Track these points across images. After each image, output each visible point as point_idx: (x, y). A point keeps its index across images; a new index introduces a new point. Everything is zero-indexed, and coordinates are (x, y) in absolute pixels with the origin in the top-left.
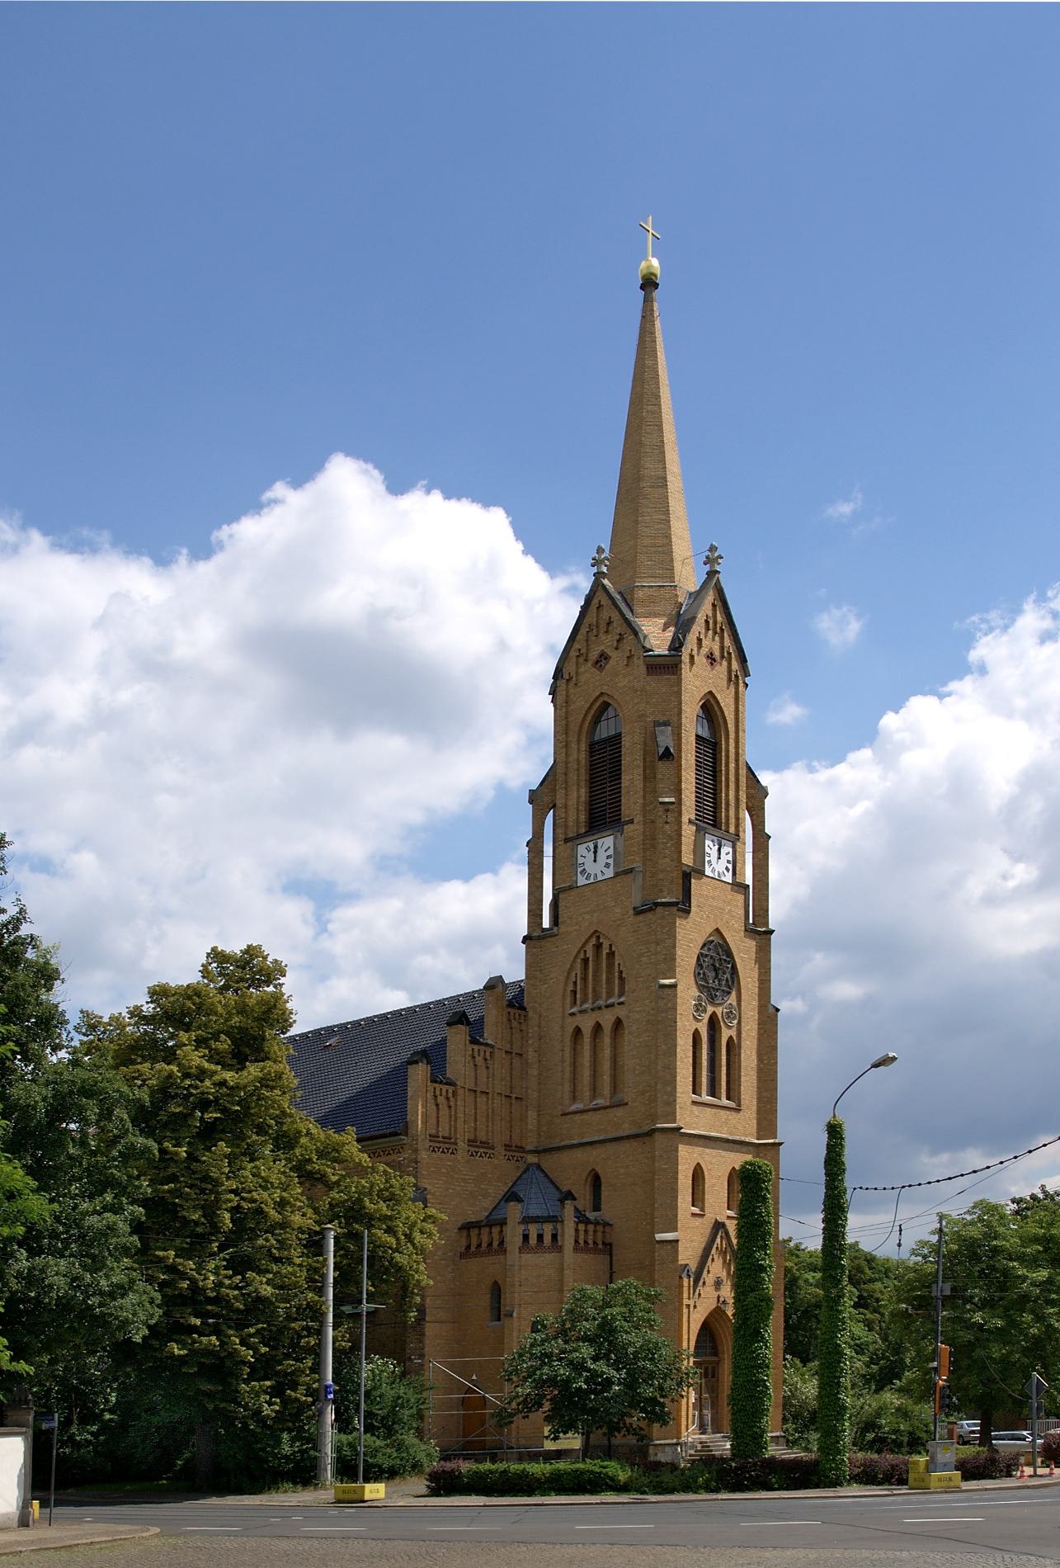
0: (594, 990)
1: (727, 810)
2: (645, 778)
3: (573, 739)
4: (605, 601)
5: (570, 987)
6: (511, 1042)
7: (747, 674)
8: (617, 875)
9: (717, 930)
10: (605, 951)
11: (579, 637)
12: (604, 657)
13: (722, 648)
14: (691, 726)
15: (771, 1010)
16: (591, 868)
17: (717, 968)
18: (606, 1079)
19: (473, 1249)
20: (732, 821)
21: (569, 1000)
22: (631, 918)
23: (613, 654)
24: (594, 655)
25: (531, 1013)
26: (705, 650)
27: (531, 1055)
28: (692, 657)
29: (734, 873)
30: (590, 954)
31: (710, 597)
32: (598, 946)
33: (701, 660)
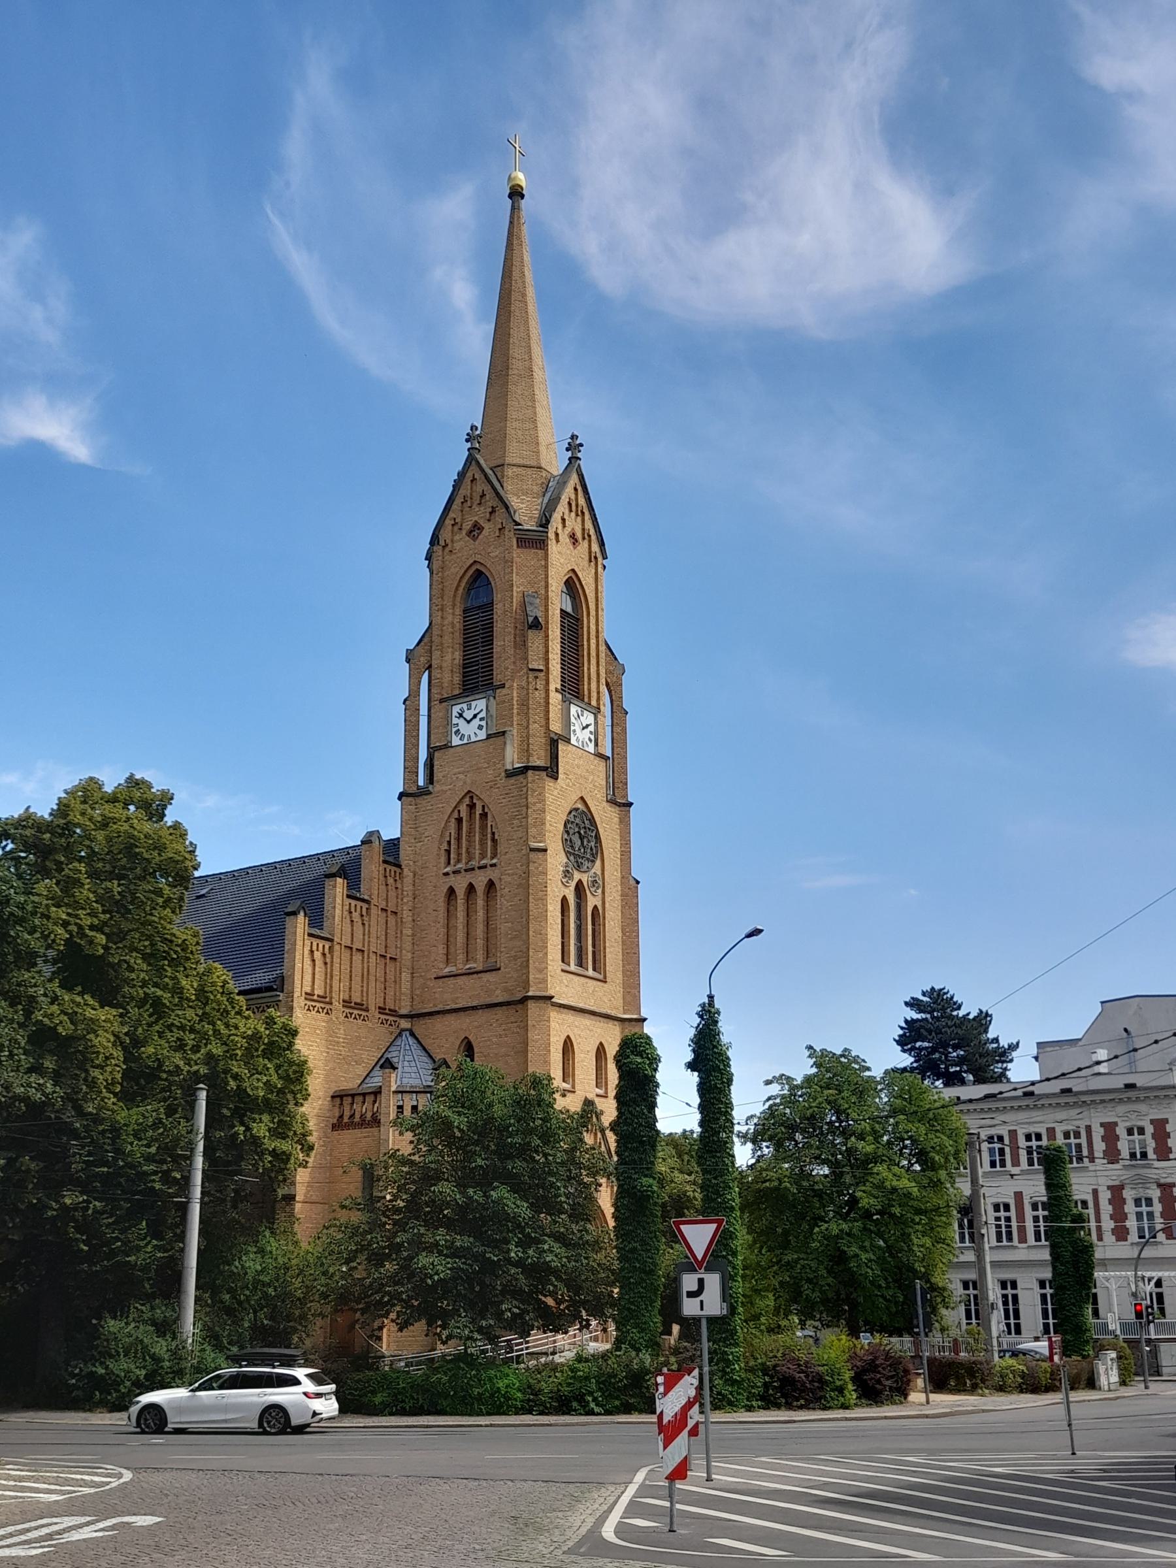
1: (589, 684)
3: (448, 602)
7: (605, 557)
8: (489, 737)
9: (582, 798)
10: (479, 811)
11: (454, 507)
12: (476, 528)
13: (583, 529)
14: (558, 601)
15: (633, 882)
17: (582, 835)
19: (346, 1120)
20: (594, 694)
21: (443, 859)
22: (503, 781)
24: (467, 526)
26: (568, 530)
27: (407, 915)
28: (557, 535)
29: (596, 745)
30: (464, 814)
31: (574, 479)
32: (472, 806)
33: (564, 538)
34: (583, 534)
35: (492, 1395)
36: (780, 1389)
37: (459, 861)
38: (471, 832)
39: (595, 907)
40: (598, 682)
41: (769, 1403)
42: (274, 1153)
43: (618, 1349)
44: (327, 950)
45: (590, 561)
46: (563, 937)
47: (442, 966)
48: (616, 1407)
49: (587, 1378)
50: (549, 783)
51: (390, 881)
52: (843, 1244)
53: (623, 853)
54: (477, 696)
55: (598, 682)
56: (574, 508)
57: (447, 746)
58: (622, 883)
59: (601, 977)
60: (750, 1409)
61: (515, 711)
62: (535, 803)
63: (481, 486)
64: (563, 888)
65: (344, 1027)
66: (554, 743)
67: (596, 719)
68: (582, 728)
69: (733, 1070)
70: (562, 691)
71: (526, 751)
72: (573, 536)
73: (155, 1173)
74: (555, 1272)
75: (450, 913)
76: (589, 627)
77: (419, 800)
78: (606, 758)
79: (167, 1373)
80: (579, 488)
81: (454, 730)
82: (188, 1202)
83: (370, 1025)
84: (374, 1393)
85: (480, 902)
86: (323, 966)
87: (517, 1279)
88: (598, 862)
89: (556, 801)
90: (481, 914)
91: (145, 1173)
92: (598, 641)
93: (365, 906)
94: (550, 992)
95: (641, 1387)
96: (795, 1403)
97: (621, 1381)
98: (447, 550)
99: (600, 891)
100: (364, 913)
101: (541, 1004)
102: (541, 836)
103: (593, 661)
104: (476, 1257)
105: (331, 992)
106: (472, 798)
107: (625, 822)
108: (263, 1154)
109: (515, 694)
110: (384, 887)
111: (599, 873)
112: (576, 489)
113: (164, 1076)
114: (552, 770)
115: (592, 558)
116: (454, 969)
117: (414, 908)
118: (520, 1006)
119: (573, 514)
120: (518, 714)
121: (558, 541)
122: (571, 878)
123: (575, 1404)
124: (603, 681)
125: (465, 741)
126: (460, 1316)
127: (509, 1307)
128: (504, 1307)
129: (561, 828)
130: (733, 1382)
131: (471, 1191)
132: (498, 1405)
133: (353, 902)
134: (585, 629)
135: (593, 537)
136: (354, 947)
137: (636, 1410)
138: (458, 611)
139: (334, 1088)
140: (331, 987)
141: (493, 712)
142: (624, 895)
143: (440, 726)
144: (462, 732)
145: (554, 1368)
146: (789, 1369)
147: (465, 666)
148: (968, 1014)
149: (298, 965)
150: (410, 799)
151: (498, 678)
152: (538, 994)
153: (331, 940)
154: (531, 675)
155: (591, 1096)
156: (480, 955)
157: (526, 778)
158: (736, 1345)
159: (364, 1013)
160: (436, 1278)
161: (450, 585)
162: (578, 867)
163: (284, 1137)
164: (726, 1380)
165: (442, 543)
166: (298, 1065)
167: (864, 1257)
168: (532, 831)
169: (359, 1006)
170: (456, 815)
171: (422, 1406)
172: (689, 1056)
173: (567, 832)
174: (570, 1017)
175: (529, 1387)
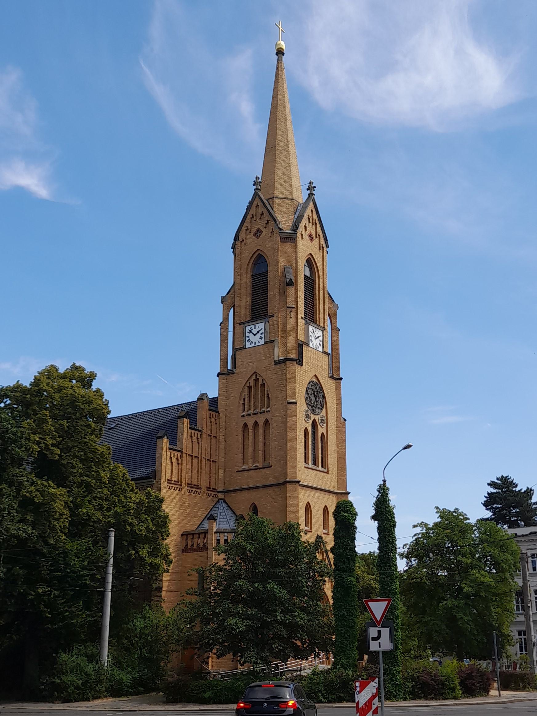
1: (319, 314)
5: (242, 401)
7: (328, 247)
8: (266, 343)
9: (315, 376)
10: (260, 382)
11: (247, 220)
12: (259, 232)
13: (316, 232)
14: (303, 271)
15: (343, 420)
17: (316, 396)
18: (261, 453)
19: (189, 547)
20: (322, 320)
21: (241, 408)
22: (273, 366)
23: (264, 230)
24: (254, 230)
25: (221, 415)
26: (308, 232)
27: (222, 438)
28: (302, 235)
29: (323, 347)
31: (311, 205)
32: (256, 380)
33: (306, 236)
37: (249, 409)
41: (415, 696)
42: (151, 565)
45: (320, 249)
46: (305, 450)
47: (240, 465)
48: (334, 699)
49: (318, 684)
50: (298, 367)
51: (213, 420)
57: (243, 348)
58: (337, 421)
59: (326, 471)
60: (405, 699)
63: (261, 209)
64: (305, 424)
66: (300, 346)
68: (316, 338)
70: (305, 318)
71: (285, 350)
72: (310, 236)
73: (87, 575)
76: (319, 285)
77: (228, 377)
78: (328, 354)
80: (314, 210)
81: (247, 339)
82: (105, 591)
84: (205, 692)
88: (324, 410)
89: (302, 377)
92: (324, 292)
93: (199, 433)
94: (299, 479)
98: (243, 243)
99: (325, 425)
101: (294, 485)
103: (322, 302)
105: (181, 479)
106: (256, 375)
107: (338, 388)
109: (280, 320)
111: (325, 415)
113: (92, 524)
114: (299, 361)
115: (321, 248)
116: (247, 467)
117: (225, 434)
118: (282, 486)
119: (311, 224)
120: (281, 331)
121: (302, 238)
122: (310, 418)
125: (253, 345)
128: (274, 646)
134: (317, 285)
135: (322, 236)
136: (194, 455)
138: (249, 276)
139: (183, 530)
140: (181, 476)
141: (268, 329)
143: (240, 337)
148: (521, 490)
151: (270, 312)
152: (292, 480)
153: (182, 452)
154: (288, 310)
155: (320, 534)
156: (261, 459)
157: (285, 365)
158: (398, 666)
159: (199, 491)
161: (245, 261)
162: (314, 412)
163: (157, 556)
168: (289, 393)
169: (196, 486)
172: (373, 513)
173: (308, 393)
174: (309, 492)
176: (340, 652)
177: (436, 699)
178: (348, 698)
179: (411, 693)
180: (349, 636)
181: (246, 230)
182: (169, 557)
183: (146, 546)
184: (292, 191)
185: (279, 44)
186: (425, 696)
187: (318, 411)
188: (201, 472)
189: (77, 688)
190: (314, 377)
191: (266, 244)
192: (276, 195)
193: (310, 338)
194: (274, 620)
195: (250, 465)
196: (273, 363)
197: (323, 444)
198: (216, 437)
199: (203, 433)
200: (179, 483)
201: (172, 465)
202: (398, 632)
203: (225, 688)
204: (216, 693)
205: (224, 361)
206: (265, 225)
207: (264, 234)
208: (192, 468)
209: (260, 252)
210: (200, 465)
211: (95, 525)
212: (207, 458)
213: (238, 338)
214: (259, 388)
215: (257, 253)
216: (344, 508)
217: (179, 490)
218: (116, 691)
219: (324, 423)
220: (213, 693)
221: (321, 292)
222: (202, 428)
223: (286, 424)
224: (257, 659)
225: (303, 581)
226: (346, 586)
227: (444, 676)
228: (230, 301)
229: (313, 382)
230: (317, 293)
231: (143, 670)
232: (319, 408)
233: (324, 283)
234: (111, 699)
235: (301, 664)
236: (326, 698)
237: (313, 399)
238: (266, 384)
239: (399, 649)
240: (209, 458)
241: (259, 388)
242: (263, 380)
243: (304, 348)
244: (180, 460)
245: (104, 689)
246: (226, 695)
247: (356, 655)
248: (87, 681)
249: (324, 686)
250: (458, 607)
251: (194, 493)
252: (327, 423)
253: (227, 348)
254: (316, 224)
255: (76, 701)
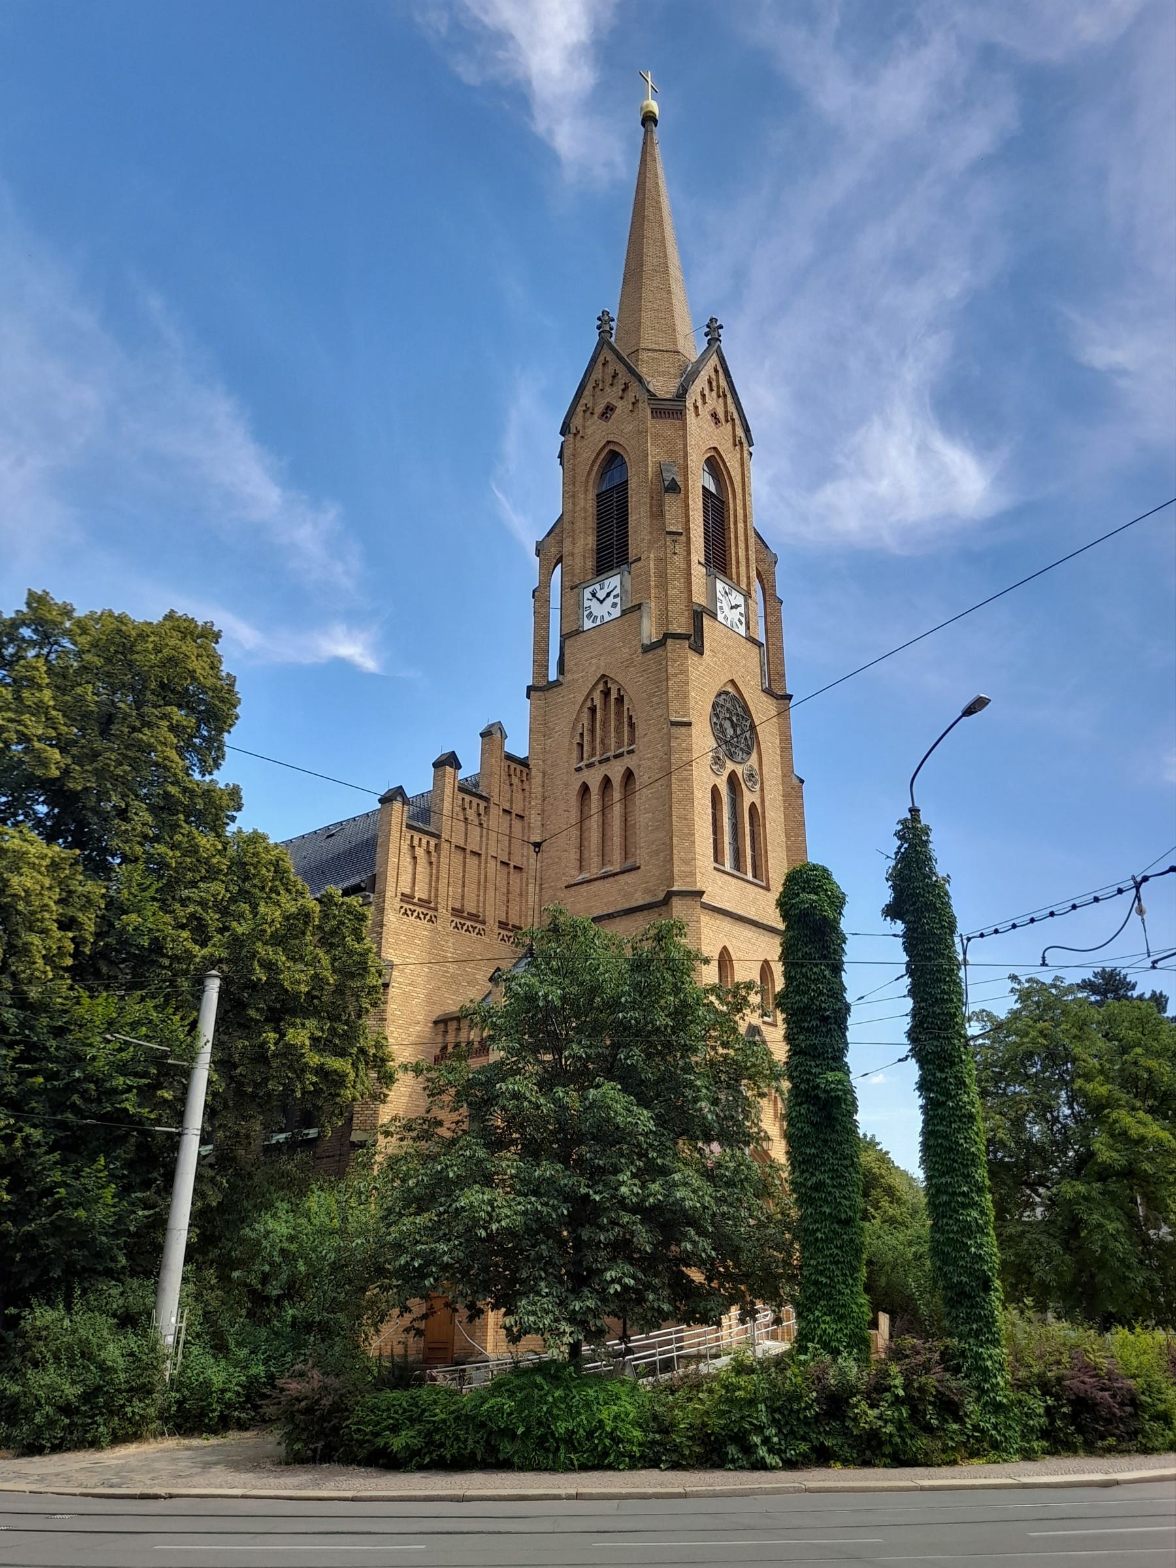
0: (602, 741)
1: (738, 567)
2: (652, 515)
3: (580, 488)
4: (610, 357)
5: (577, 740)
6: (511, 801)
7: (751, 444)
8: (624, 613)
9: (732, 681)
10: (614, 695)
11: (586, 393)
12: (610, 409)
13: (726, 412)
14: (700, 480)
15: (796, 781)
16: (598, 610)
17: (735, 726)
18: (617, 840)
19: (450, 1050)
21: (575, 754)
22: (639, 658)
23: (619, 404)
24: (599, 409)
25: (534, 772)
28: (696, 408)
29: (748, 628)
30: (598, 702)
31: (714, 360)
32: (606, 693)
33: (705, 411)
34: (726, 416)
35: (590, 1435)
36: (1073, 1418)
37: (593, 755)
38: (605, 723)
39: (753, 803)
40: (748, 567)
41: (1057, 1443)
42: (321, 1071)
43: (803, 1350)
44: (432, 848)
45: (735, 445)
46: (715, 833)
47: (574, 872)
48: (804, 1455)
49: (752, 1403)
50: (692, 657)
51: (515, 781)
52: (1081, 1210)
53: (783, 750)
54: (610, 573)
55: (748, 567)
56: (715, 389)
57: (578, 632)
58: (783, 783)
59: (764, 884)
60: (1028, 1455)
61: (653, 583)
62: (676, 675)
63: (614, 366)
64: (713, 776)
65: (454, 943)
66: (698, 615)
67: (746, 601)
68: (730, 608)
69: (956, 910)
70: (708, 563)
71: (664, 617)
72: (714, 415)
73: (129, 1089)
74: (692, 1220)
75: (583, 818)
76: (735, 511)
77: (548, 694)
78: (760, 645)
79: (119, 1391)
80: (719, 368)
81: (586, 613)
82: (180, 1135)
83: (488, 940)
84: (395, 1429)
85: (617, 795)
86: (427, 865)
87: (632, 1233)
88: (754, 755)
89: (702, 679)
90: (617, 809)
91: (115, 1091)
92: (746, 526)
93: (483, 804)
94: (699, 886)
95: (843, 1418)
96: (1100, 1444)
97: (809, 1407)
98: (579, 437)
99: (758, 787)
100: (482, 811)
101: (689, 901)
102: (685, 708)
103: (742, 545)
104: (568, 1197)
105: (436, 896)
106: (606, 683)
107: (783, 714)
108: (303, 1071)
109: (652, 566)
110: (507, 787)
111: (756, 767)
112: (716, 371)
113: (167, 962)
115: (737, 443)
116: (587, 875)
117: (543, 811)
118: (664, 908)
119: (714, 394)
120: (656, 586)
121: (697, 415)
122: (723, 766)
123: (732, 1450)
124: (753, 566)
125: (599, 623)
126: (538, 1293)
127: (618, 1275)
128: (608, 1275)
129: (710, 709)
130: (998, 1408)
131: (560, 1092)
132: (599, 1453)
133: (468, 798)
134: (731, 512)
135: (737, 422)
136: (469, 848)
137: (837, 1458)
138: (591, 495)
139: (438, 1012)
140: (437, 890)
141: (628, 587)
142: (786, 795)
143: (573, 608)
144: (595, 614)
145: (697, 1384)
146: (1083, 1384)
147: (599, 551)
149: (393, 860)
150: (539, 694)
151: (632, 553)
152: (684, 888)
153: (438, 837)
154: (669, 538)
156: (617, 855)
157: (666, 649)
158: (996, 1343)
159: (479, 926)
160: (494, 1227)
161: (583, 470)
162: (731, 756)
163: (342, 1053)
164: (986, 1404)
165: (573, 430)
166: (361, 955)
167: (1111, 1227)
168: (674, 705)
169: (474, 917)
170: (589, 704)
171: (473, 1453)
172: (886, 896)
173: (717, 715)
174: (726, 924)
175: (655, 1417)
176: (816, 1300)
177: (1121, 1452)
178: (847, 1452)
179: (1045, 1434)
180: (840, 1248)
181: (584, 411)
182: (735, 1311)
183: (312, 1023)
184: (674, 340)
185: (647, 106)
186: (1085, 1441)
187: (740, 755)
188: (485, 887)
189: (66, 1409)
190: (729, 685)
191: (621, 429)
192: (643, 346)
193: (719, 604)
194: (613, 1197)
195: (595, 871)
196: (640, 650)
197: (756, 828)
198: (522, 817)
199: (492, 805)
200: (432, 905)
201: (415, 863)
202: (988, 1235)
203: (457, 1418)
204: (429, 1434)
205: (541, 663)
206: (620, 393)
207: (618, 411)
208: (464, 876)
209: (611, 447)
210: (483, 871)
211: (175, 965)
212: (500, 858)
213: (568, 616)
214: (612, 708)
215: (606, 451)
216: (808, 881)
217: (430, 920)
218: (191, 1417)
219: (755, 783)
220: (420, 1432)
221: (741, 525)
222: (489, 793)
223: (671, 771)
224: (556, 1320)
225: (698, 1083)
226: (823, 1096)
227: (1134, 1377)
228: (553, 549)
229: (727, 693)
230: (732, 526)
231: (283, 1356)
232: (741, 749)
233: (745, 509)
234: (171, 1443)
235: (717, 1339)
236: (779, 1452)
237: (730, 732)
238: (626, 699)
239: (996, 1290)
240: (505, 860)
241: (612, 708)
242: (619, 690)
243: (706, 621)
244: (433, 853)
245: (152, 1411)
246: (457, 1439)
247: (865, 1309)
248: (98, 1388)
249: (771, 1410)
250: (1085, 1198)
251: (467, 930)
252: (762, 783)
253: (546, 638)
254: (725, 396)
255: (57, 1448)
